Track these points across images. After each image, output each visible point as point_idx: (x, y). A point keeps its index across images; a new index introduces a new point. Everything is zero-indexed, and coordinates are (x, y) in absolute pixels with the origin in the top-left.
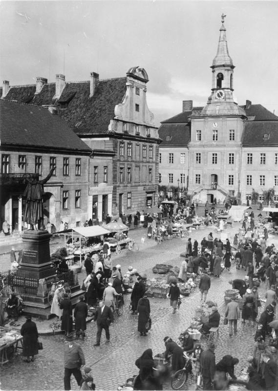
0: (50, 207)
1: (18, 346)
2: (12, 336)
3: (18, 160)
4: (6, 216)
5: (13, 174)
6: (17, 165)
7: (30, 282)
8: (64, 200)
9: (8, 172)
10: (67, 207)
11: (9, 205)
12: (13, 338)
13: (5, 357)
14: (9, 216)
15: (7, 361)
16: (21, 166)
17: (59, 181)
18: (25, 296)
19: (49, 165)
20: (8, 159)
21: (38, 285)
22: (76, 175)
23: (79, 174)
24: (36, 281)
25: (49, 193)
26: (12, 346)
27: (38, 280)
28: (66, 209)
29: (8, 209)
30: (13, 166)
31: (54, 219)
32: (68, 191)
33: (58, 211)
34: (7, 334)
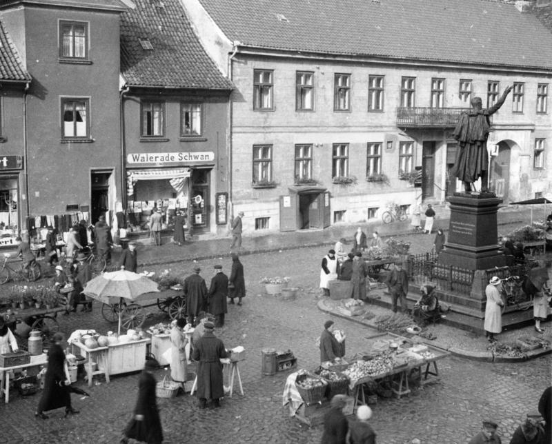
0: (511, 164)
1: (430, 370)
2: (418, 353)
3: (458, 87)
4: (437, 174)
5: (449, 108)
6: (457, 96)
7: (439, 269)
8: (537, 153)
9: (441, 106)
10: (541, 166)
11: (442, 152)
12: (419, 357)
13: (404, 384)
14: (441, 175)
15: (408, 391)
16: (463, 96)
17: (529, 122)
18: (450, 295)
19: (429, 94)
20: (441, 85)
21: (472, 280)
22: (514, 112)
23: (520, 110)
24: (470, 274)
25: (511, 141)
26: (417, 369)
27: (474, 271)
28: (539, 169)
29: (440, 164)
30: (450, 96)
31: (517, 184)
32: (544, 139)
33: (525, 171)
34: (411, 349)
